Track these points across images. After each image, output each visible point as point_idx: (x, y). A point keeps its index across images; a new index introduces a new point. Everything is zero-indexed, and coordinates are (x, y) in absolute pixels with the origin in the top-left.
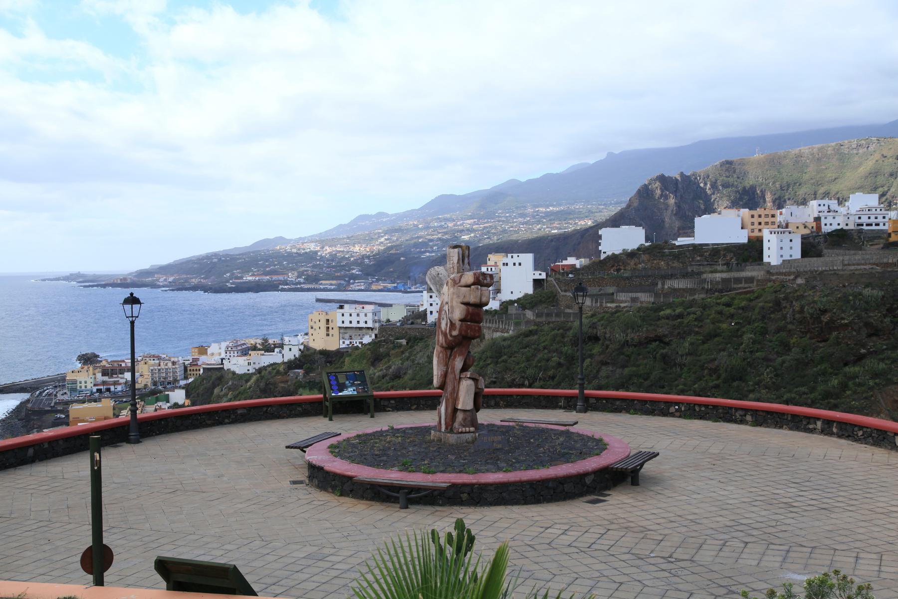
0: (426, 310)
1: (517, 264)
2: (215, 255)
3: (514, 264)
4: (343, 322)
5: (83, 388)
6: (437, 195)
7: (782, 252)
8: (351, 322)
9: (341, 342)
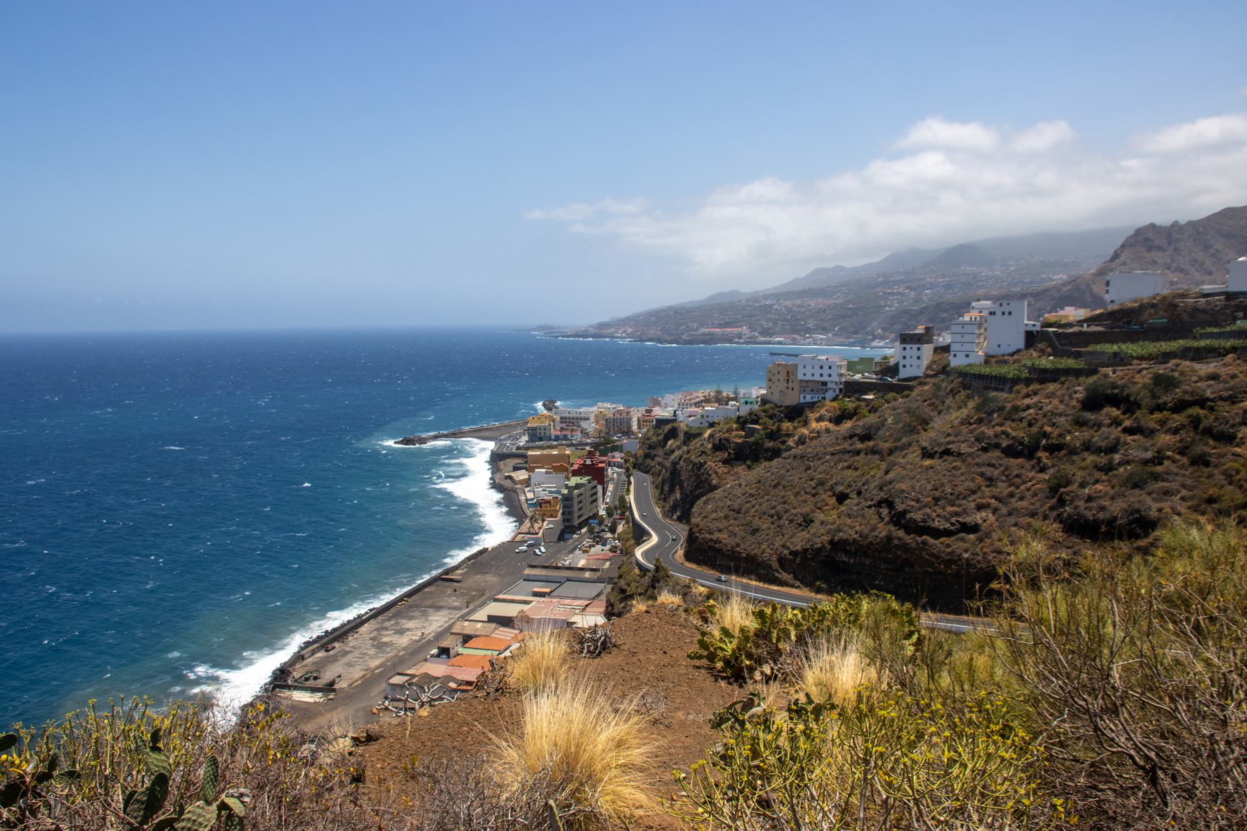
2: (670, 308)
7: (918, 353)
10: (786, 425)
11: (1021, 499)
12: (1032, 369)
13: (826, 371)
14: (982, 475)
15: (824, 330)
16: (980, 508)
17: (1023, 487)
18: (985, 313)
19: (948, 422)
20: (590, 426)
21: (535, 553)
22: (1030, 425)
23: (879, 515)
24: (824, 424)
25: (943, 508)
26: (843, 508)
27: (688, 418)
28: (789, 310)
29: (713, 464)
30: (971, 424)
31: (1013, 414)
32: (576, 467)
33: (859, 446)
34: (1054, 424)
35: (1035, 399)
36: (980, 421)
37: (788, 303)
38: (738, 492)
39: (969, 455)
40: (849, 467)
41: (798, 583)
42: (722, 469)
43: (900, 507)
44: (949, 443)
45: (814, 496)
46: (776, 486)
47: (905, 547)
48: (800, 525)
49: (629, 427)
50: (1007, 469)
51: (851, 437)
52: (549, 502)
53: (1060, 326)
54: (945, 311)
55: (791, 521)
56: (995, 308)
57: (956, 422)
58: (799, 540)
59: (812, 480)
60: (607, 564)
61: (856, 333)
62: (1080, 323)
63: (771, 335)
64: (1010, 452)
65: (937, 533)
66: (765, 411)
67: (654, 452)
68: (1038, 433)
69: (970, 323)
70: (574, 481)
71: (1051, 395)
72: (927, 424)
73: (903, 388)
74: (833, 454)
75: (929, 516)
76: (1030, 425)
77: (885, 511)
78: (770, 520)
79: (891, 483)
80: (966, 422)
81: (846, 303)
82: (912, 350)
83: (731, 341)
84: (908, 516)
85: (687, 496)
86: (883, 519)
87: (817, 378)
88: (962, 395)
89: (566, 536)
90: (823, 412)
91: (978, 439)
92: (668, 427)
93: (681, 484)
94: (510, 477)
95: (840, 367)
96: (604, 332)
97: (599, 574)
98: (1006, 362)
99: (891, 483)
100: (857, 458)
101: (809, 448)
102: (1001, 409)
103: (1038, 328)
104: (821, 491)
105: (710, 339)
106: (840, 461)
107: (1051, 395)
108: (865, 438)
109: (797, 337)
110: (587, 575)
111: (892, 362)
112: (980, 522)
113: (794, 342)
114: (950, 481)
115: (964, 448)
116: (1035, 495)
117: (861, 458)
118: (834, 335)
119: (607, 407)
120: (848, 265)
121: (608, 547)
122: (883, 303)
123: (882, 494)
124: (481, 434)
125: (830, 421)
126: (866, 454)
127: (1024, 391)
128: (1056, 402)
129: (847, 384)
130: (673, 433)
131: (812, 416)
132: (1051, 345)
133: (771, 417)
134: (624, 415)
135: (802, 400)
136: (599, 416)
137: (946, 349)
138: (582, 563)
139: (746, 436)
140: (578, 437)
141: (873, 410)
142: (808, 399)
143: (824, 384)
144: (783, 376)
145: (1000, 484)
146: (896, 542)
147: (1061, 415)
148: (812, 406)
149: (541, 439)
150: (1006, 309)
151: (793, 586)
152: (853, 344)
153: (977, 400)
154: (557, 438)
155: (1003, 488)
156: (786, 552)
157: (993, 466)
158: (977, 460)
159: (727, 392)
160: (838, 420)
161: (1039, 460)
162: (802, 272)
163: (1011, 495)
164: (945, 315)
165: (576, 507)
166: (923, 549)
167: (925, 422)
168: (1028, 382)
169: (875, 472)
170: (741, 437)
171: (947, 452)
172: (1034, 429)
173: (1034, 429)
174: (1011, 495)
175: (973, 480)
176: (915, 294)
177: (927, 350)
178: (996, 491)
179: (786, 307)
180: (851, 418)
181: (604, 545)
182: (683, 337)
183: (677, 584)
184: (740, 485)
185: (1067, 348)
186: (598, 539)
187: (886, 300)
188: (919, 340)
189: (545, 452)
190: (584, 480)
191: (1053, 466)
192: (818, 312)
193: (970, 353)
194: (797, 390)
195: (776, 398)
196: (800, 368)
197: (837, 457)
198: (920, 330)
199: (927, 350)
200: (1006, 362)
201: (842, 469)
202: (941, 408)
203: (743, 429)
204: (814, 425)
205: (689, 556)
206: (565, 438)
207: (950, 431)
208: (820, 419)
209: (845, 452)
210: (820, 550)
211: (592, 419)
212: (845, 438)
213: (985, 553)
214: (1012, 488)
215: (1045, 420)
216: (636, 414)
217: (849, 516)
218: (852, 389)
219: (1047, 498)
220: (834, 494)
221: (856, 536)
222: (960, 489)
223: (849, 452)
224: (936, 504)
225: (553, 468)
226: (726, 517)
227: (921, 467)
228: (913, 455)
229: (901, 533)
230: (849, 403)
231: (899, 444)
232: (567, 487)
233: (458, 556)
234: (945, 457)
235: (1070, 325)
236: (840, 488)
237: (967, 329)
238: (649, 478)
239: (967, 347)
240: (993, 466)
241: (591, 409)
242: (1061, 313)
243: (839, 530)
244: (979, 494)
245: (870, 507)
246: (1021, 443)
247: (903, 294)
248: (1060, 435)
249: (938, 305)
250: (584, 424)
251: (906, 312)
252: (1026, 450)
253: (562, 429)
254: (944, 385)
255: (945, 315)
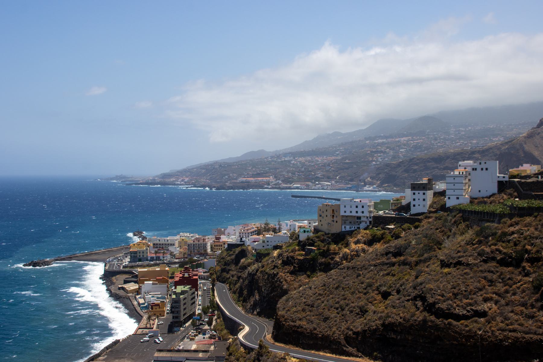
0: (410, 203)
1: (484, 169)
2: (216, 163)
3: (482, 169)
4: (345, 212)
5: (141, 256)
6: (245, 152)
7: (424, 197)
8: (351, 212)
9: (343, 227)
10: (333, 247)
11: (514, 294)
12: (512, 207)
13: (360, 209)
14: (485, 278)
15: (329, 179)
16: (486, 300)
17: (514, 286)
18: (469, 169)
19: (457, 242)
20: (176, 250)
21: (155, 342)
22: (516, 245)
23: (416, 306)
24: (361, 246)
25: (461, 300)
26: (387, 302)
27: (252, 242)
28: (303, 164)
29: (284, 275)
30: (473, 245)
31: (503, 238)
32: (177, 279)
33: (394, 260)
34: (532, 244)
35: (517, 228)
36: (480, 242)
37: (302, 159)
38: (310, 292)
39: (475, 265)
40: (388, 274)
41: (360, 354)
42: (289, 278)
43: (431, 300)
44: (459, 257)
45: (365, 294)
46: (337, 288)
47: (436, 327)
48: (358, 314)
49: (206, 250)
50: (502, 274)
51: (387, 254)
52: (158, 305)
53: (522, 177)
54: (416, 164)
55: (351, 312)
56: (476, 165)
57: (463, 243)
58: (359, 325)
59: (362, 283)
60: (212, 348)
61: (352, 180)
62: (536, 175)
63: (291, 182)
64: (503, 263)
65: (458, 318)
66: (318, 237)
67: (228, 268)
68: (522, 250)
69: (459, 176)
70: (179, 289)
71: (529, 225)
72: (441, 244)
73: (415, 220)
74: (375, 266)
75: (452, 306)
76: (516, 245)
77: (419, 303)
78: (336, 311)
79: (421, 284)
80: (470, 243)
81: (348, 160)
82: (419, 194)
83: (262, 187)
84: (437, 306)
85: (264, 297)
86: (418, 309)
87: (354, 214)
88: (462, 226)
89: (176, 329)
90: (359, 237)
91: (479, 254)
92: (238, 250)
93: (259, 290)
94: (123, 288)
95: (369, 206)
96: (167, 180)
97: (209, 354)
98: (485, 203)
99: (421, 284)
100: (394, 268)
101: (357, 262)
102: (494, 234)
103: (507, 179)
104: (370, 291)
105: (247, 186)
106: (381, 270)
107: (529, 225)
108: (398, 253)
109: (310, 183)
110: (201, 355)
111: (404, 202)
112: (487, 310)
113: (308, 187)
114: (463, 282)
115: (471, 260)
116: (524, 291)
117: (396, 268)
118: (336, 182)
119: (189, 236)
120: (344, 131)
121: (207, 336)
122: (371, 159)
123: (416, 292)
124: (92, 257)
125: (365, 243)
126: (399, 265)
127: (509, 222)
128: (532, 229)
129: (374, 217)
130: (243, 254)
131: (352, 240)
132: (517, 190)
133: (323, 241)
134: (201, 242)
135: (343, 230)
136: (182, 243)
137: (443, 193)
138: (194, 347)
139: (306, 255)
140: (168, 258)
141: (397, 237)
142: (348, 228)
143: (359, 218)
144: (329, 213)
145: (498, 284)
146: (430, 324)
147: (537, 238)
148: (351, 233)
149: (140, 260)
150: (484, 166)
151: (357, 356)
152: (350, 189)
153: (476, 228)
154: (152, 259)
155: (500, 287)
156: (350, 333)
157: (492, 272)
158: (480, 268)
159: (273, 224)
160: (370, 243)
161: (524, 268)
162: (310, 136)
163: (507, 292)
164: (416, 167)
165: (182, 307)
166: (449, 328)
167: (439, 244)
168: (511, 216)
169: (408, 278)
170: (302, 255)
171: (459, 263)
172: (519, 248)
173: (519, 248)
174: (507, 292)
175: (479, 282)
176: (412, 155)
177: (430, 194)
178: (495, 289)
179: (300, 162)
180: (379, 241)
181: (204, 334)
182: (228, 185)
183: (276, 357)
184: (310, 288)
185: (529, 192)
186: (200, 331)
187: (373, 157)
188: (424, 187)
189: (151, 269)
190: (187, 288)
191: (535, 272)
192: (324, 166)
193: (460, 196)
194: (340, 222)
195: (325, 228)
196: (342, 207)
197: (378, 268)
198: (425, 181)
199: (430, 194)
200: (485, 203)
201: (383, 275)
202: (449, 233)
203: (303, 250)
204: (353, 246)
205: (277, 338)
206: (158, 258)
207: (460, 249)
208: (357, 242)
209: (383, 264)
210: (375, 330)
211: (177, 244)
212: (382, 255)
213: (493, 331)
214: (507, 287)
215: (526, 241)
216: (210, 241)
217: (394, 307)
218: (378, 221)
219: (533, 293)
220: (380, 293)
221: (401, 320)
222: (471, 287)
223: (387, 264)
224: (455, 298)
225: (157, 280)
226: (303, 310)
227: (442, 273)
228: (435, 266)
229: (433, 318)
230: (378, 231)
231: (422, 258)
232: (175, 293)
233: (100, 346)
234: (458, 267)
235: (529, 177)
236: (384, 289)
237: (457, 180)
238: (226, 286)
239: (457, 192)
240: (492, 272)
241: (175, 238)
242: (521, 168)
243: (388, 316)
244: (484, 291)
245: (408, 300)
246: (510, 257)
247: (384, 152)
248: (538, 251)
249: (411, 160)
250: (171, 249)
251: (388, 165)
252: (513, 262)
253: (156, 253)
254: (449, 218)
255: (416, 167)
